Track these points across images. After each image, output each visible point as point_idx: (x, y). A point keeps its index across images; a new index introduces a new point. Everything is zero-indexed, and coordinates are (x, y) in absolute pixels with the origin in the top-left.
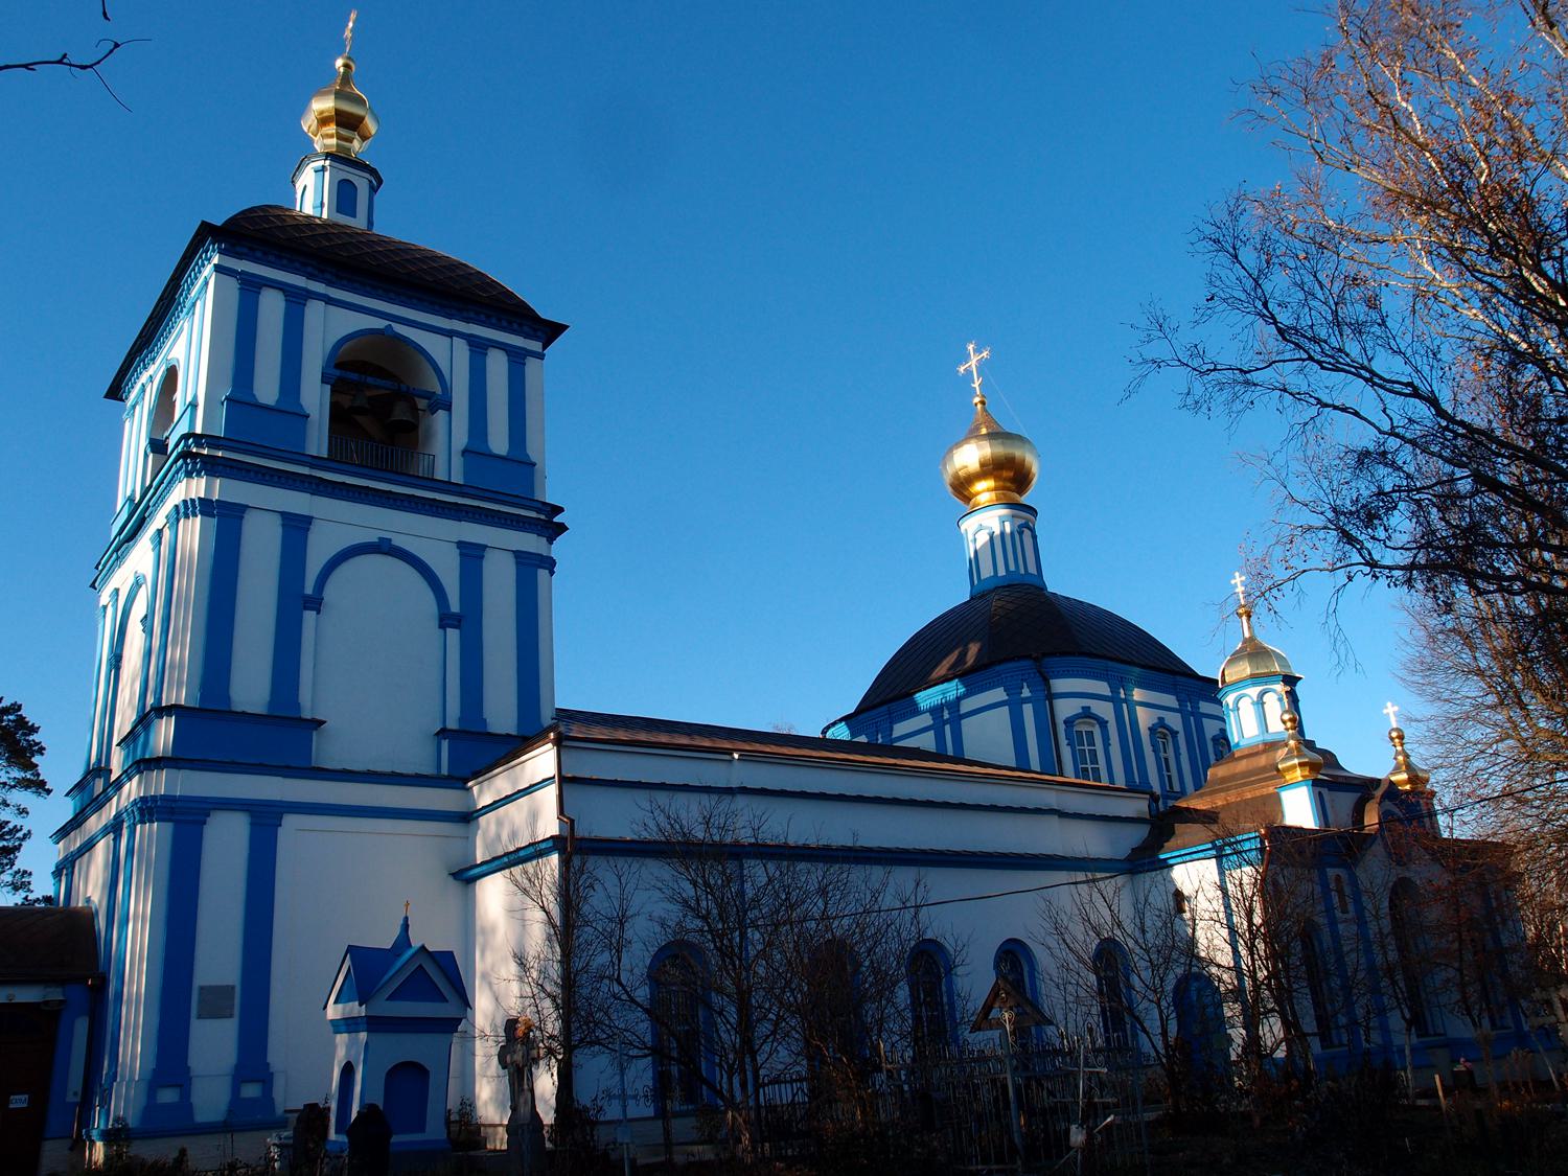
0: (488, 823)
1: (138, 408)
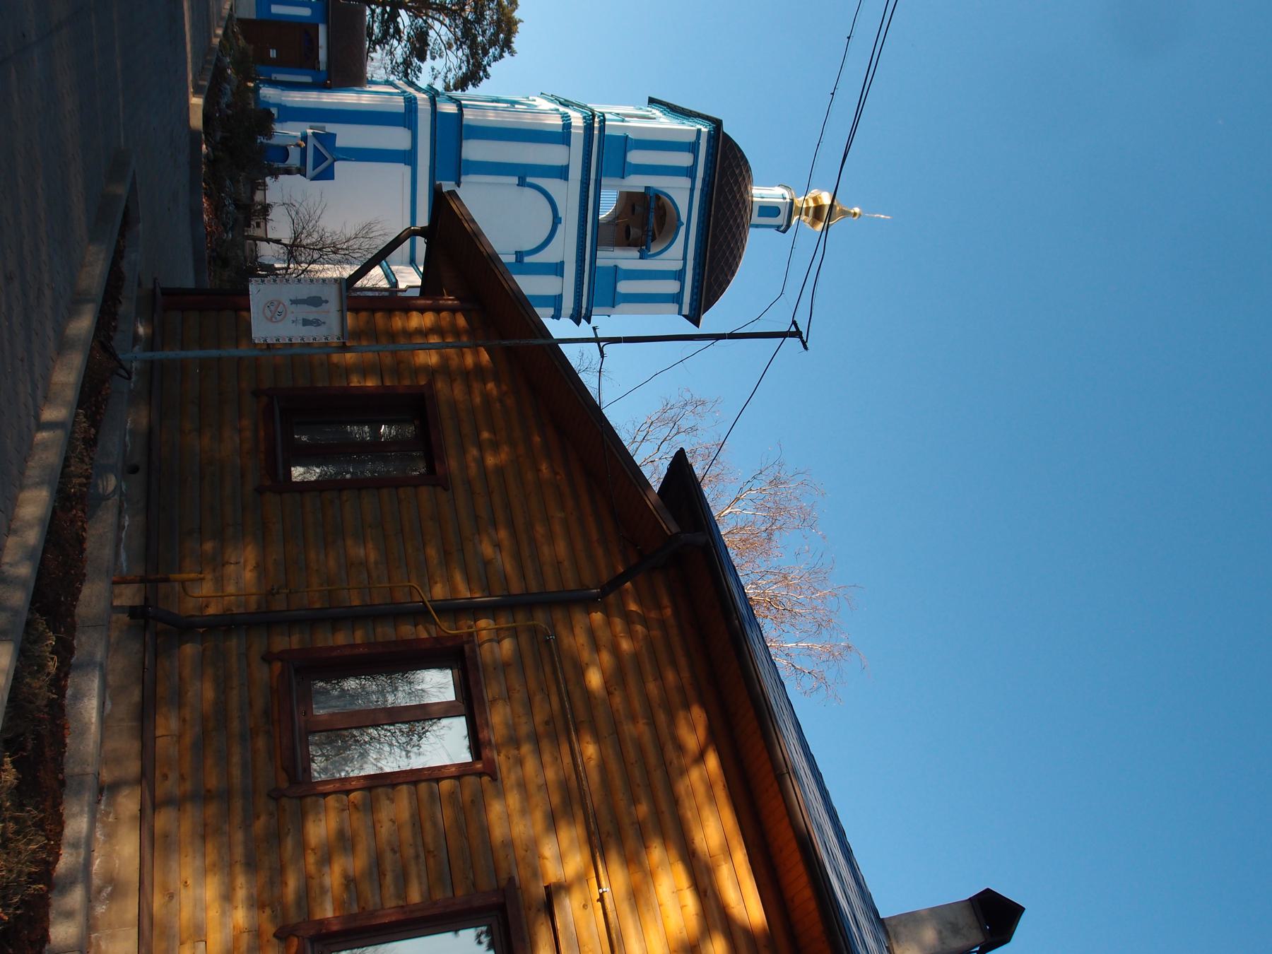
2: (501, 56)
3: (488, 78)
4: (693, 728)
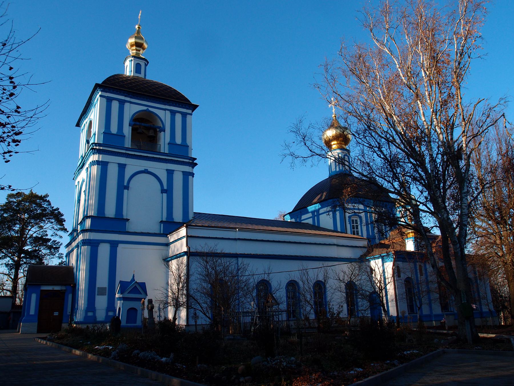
0: (172, 246)
1: (84, 130)
2: (49, 201)
3: (59, 208)
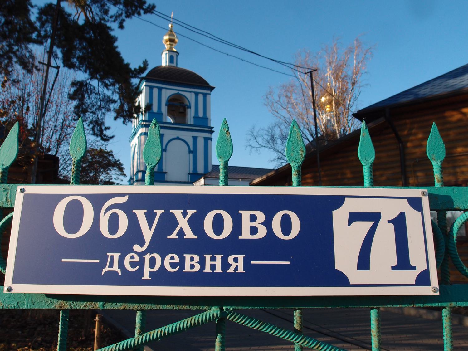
2: (112, 155)
4: (453, 116)
